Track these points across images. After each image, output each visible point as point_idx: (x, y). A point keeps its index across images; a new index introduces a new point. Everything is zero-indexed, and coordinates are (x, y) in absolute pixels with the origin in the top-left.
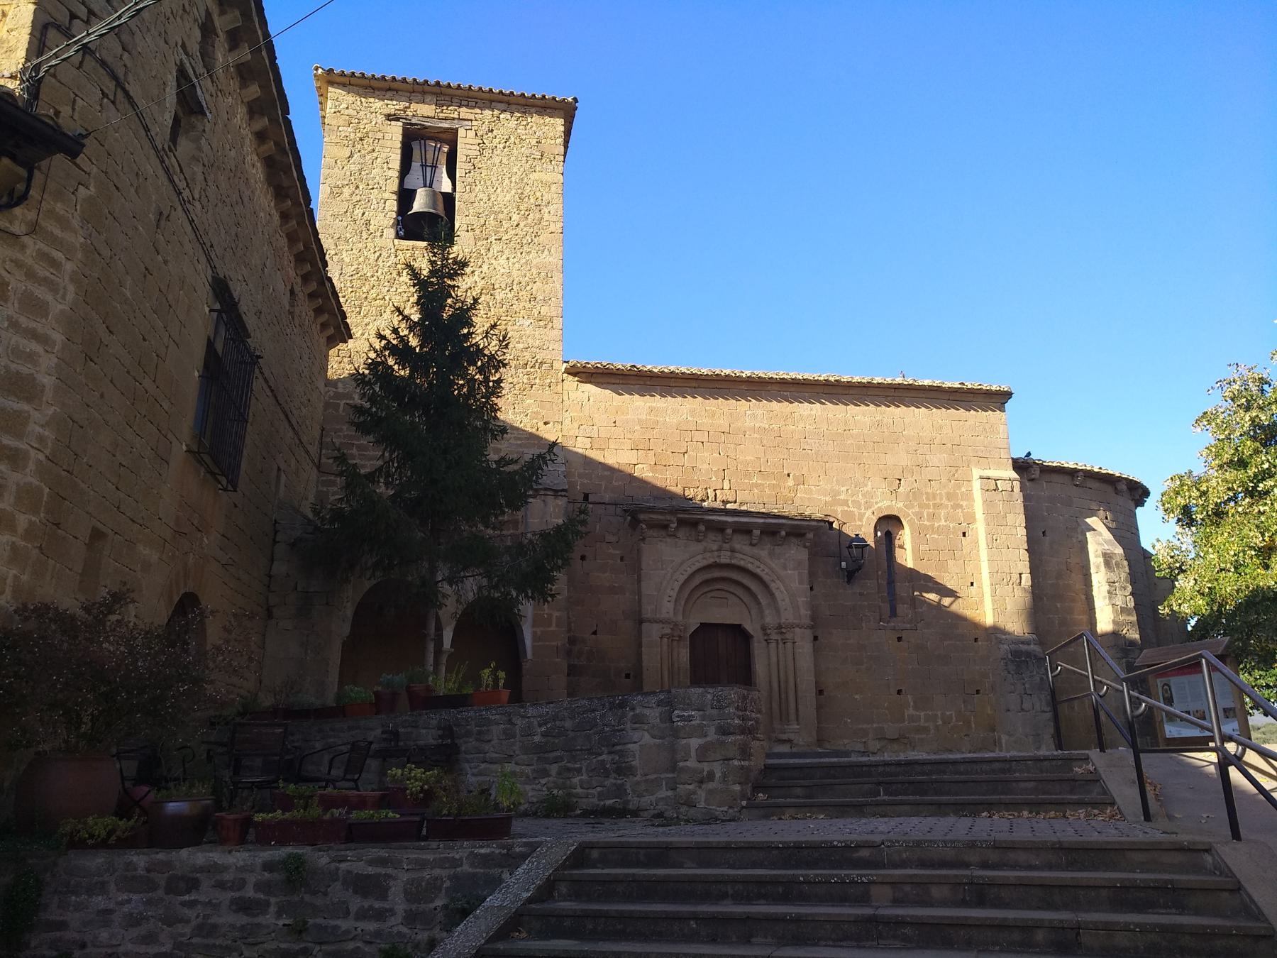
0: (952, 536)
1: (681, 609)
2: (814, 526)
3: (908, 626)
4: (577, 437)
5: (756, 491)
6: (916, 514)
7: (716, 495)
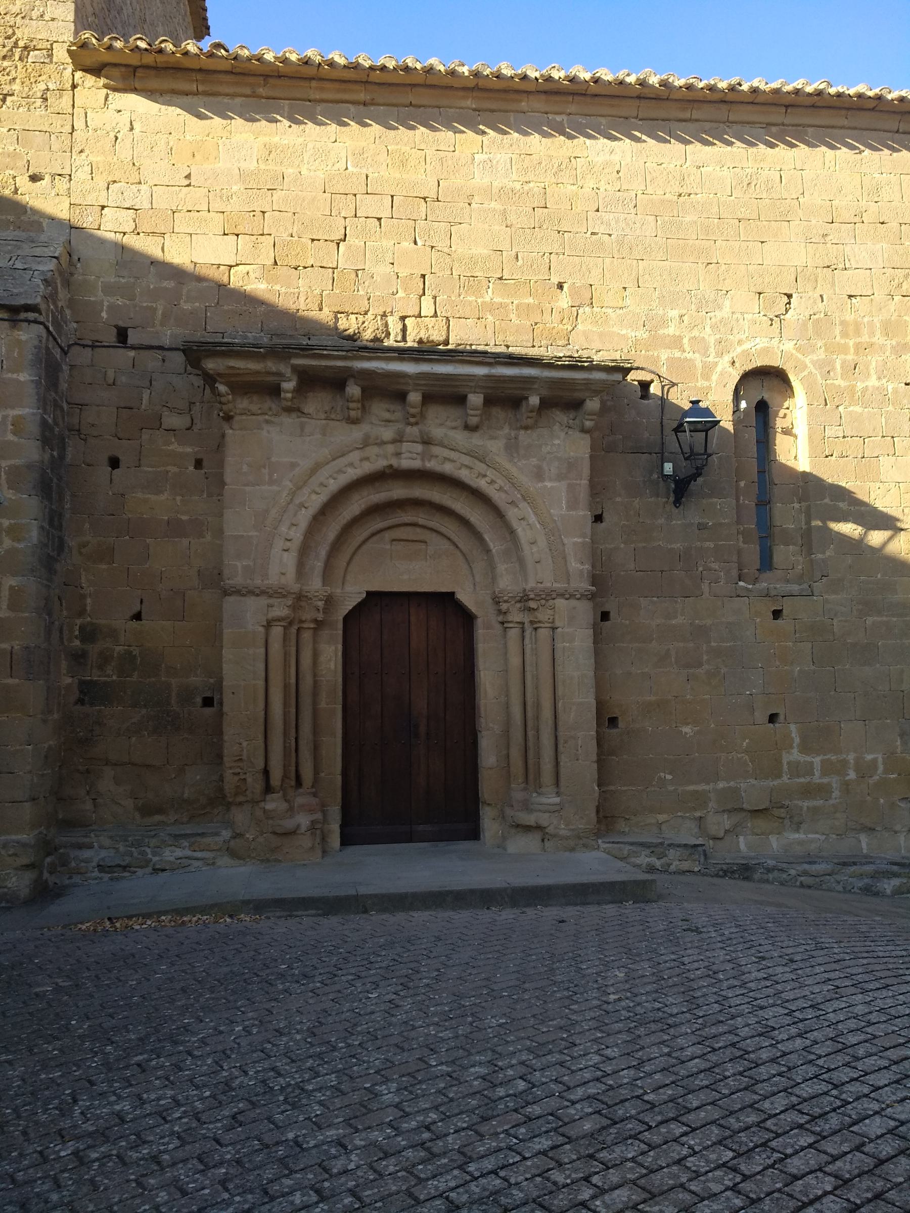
0: (891, 408)
1: (320, 565)
2: (603, 381)
3: (795, 588)
4: (103, 207)
5: (490, 318)
6: (819, 365)
7: (404, 330)
